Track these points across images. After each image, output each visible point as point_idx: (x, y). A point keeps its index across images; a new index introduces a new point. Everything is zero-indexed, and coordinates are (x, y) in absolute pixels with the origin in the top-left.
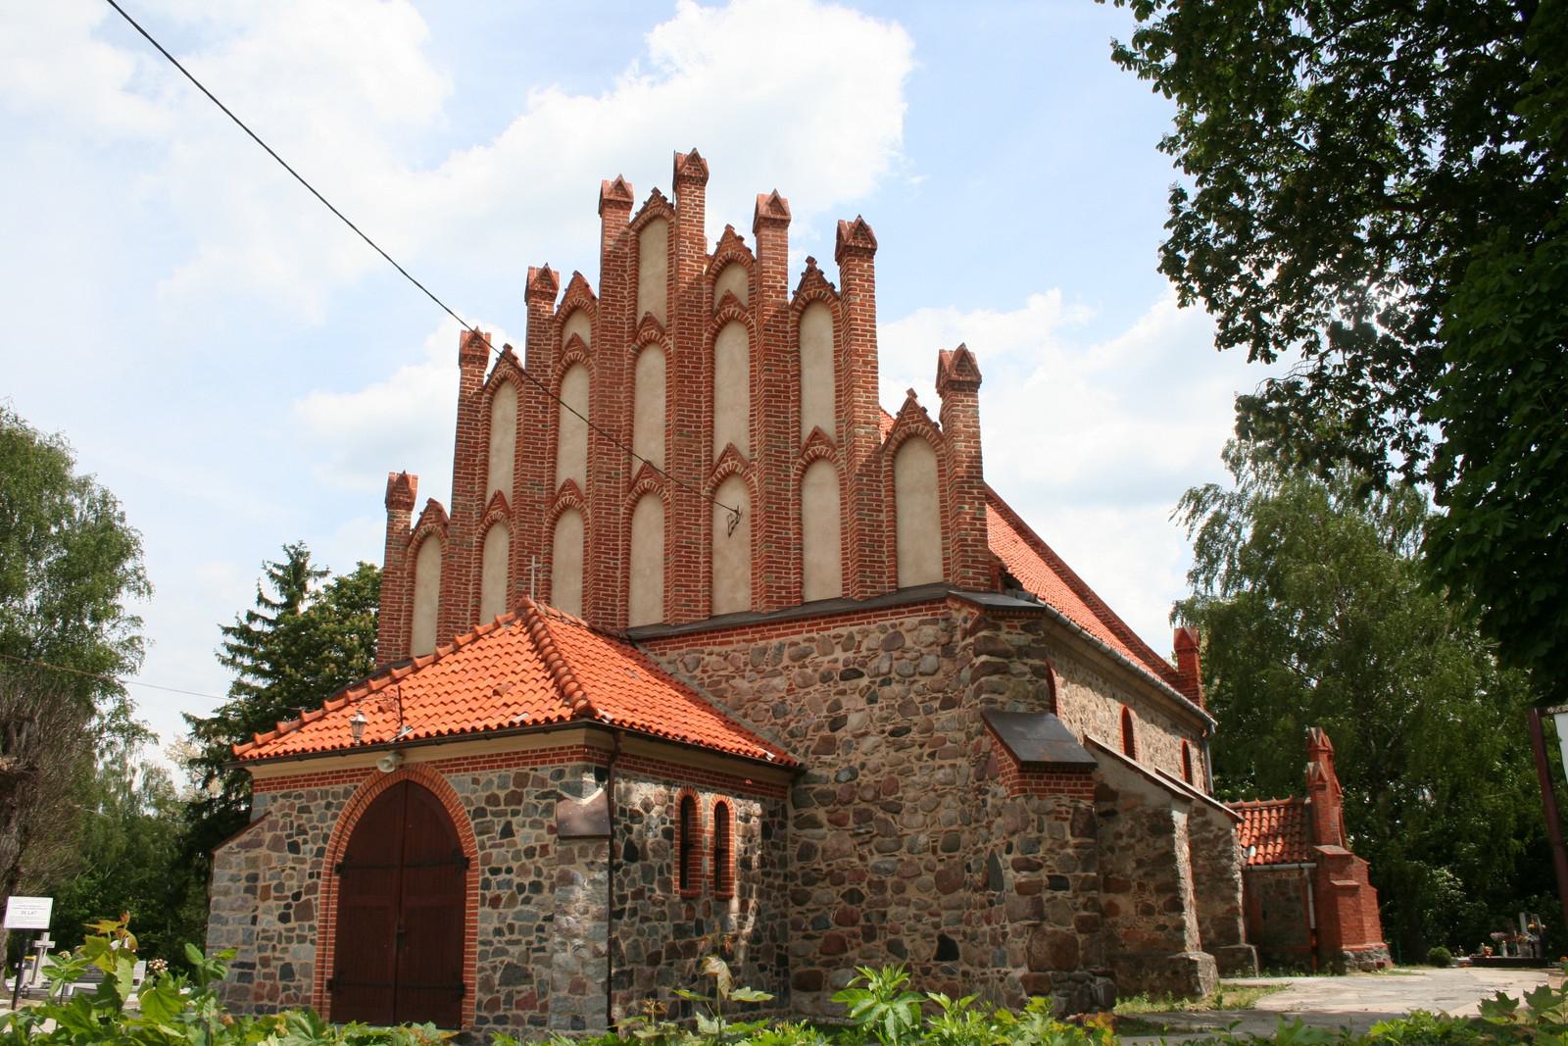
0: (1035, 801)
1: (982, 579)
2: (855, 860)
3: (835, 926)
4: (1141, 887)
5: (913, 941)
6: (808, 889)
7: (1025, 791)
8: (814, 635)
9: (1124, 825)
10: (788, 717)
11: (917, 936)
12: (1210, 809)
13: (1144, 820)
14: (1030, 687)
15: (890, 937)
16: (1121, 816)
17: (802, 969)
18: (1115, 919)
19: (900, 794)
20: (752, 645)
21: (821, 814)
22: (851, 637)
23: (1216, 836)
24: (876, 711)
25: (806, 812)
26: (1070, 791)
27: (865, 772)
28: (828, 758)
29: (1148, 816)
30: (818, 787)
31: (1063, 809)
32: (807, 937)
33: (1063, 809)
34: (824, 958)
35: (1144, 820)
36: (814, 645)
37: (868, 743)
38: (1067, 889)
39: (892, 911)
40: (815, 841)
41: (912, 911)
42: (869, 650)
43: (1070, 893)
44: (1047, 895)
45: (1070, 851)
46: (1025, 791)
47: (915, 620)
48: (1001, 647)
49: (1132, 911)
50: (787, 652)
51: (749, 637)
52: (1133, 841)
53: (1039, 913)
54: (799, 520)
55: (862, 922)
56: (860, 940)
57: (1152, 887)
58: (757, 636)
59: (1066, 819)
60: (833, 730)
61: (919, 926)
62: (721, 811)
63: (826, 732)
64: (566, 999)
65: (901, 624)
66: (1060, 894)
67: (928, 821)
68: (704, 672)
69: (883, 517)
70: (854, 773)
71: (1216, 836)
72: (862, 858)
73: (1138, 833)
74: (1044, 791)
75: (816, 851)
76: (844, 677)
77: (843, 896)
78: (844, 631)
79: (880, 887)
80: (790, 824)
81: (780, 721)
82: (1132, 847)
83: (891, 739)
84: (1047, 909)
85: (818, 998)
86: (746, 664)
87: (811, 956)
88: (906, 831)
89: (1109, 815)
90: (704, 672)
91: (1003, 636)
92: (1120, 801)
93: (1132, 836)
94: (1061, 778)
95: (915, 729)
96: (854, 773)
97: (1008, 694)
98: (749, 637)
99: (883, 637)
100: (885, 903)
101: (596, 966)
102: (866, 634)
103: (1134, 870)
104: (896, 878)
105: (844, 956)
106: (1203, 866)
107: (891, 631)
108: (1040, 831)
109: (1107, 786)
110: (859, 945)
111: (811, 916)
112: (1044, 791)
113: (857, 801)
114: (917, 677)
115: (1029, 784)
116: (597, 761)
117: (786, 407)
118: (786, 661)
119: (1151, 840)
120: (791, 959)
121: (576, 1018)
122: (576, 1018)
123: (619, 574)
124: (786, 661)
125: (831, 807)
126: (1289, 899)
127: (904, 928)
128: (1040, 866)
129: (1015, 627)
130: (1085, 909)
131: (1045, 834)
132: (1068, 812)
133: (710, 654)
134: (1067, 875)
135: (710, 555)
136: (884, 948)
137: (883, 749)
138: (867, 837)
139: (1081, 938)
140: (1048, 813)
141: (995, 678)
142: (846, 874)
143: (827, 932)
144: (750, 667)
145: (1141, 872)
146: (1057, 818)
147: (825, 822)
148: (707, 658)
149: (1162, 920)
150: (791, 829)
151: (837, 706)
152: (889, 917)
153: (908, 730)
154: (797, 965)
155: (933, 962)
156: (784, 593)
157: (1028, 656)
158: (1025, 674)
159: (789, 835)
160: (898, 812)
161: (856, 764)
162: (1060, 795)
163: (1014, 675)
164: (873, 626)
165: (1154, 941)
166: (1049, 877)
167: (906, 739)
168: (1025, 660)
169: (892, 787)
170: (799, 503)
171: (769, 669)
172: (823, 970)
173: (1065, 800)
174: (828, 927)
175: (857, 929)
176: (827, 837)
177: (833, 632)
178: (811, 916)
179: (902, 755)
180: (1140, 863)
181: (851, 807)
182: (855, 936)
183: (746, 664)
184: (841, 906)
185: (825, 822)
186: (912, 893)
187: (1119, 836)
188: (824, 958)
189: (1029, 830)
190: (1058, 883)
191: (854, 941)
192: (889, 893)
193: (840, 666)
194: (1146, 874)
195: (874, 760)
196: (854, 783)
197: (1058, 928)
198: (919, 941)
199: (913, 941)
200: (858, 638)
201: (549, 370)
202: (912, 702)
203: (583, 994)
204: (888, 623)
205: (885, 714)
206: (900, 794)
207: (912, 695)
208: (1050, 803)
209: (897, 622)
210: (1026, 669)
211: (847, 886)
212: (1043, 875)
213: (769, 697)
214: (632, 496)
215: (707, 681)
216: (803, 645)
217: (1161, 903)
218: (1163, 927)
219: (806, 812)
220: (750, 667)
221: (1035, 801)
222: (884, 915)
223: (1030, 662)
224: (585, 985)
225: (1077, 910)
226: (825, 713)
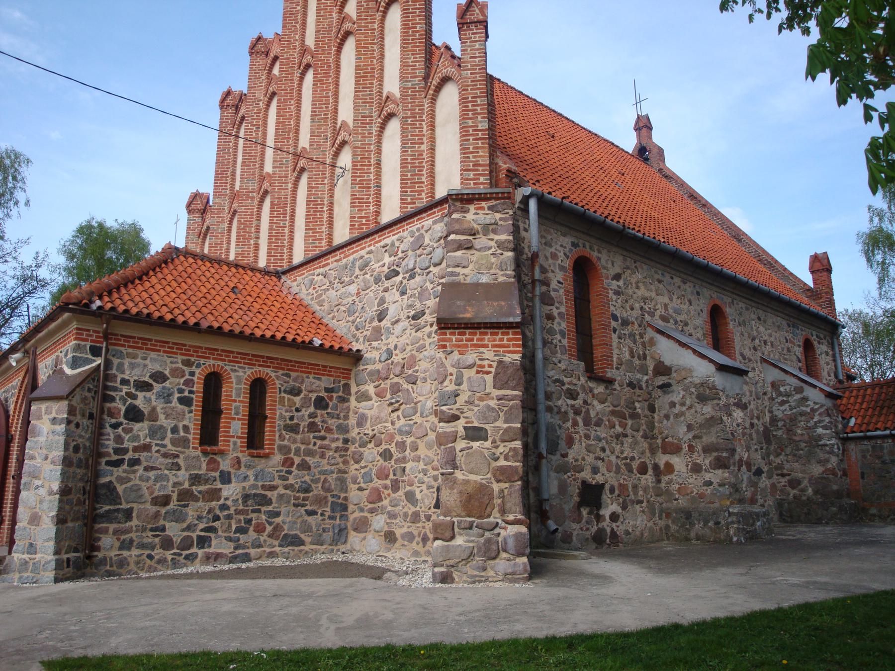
0: (456, 356)
1: (482, 179)
2: (389, 424)
3: (376, 480)
4: (691, 448)
5: (421, 491)
6: (362, 450)
7: (444, 347)
8: (372, 248)
9: (676, 396)
10: (356, 315)
11: (424, 487)
12: (805, 386)
13: (693, 390)
14: (493, 260)
15: (408, 488)
16: (674, 388)
17: (357, 514)
18: (670, 477)
19: (417, 368)
20: (340, 263)
21: (370, 389)
22: (393, 244)
23: (812, 410)
24: (405, 301)
25: (363, 388)
26: (493, 346)
27: (397, 352)
28: (375, 344)
29: (695, 386)
30: (370, 367)
31: (486, 363)
32: (361, 489)
33: (486, 363)
34: (370, 506)
35: (693, 390)
36: (371, 256)
37: (398, 328)
38: (486, 439)
39: (409, 466)
40: (366, 412)
41: (422, 466)
42: (403, 252)
43: (488, 444)
44: (461, 444)
45: (493, 403)
46: (444, 347)
47: (430, 222)
48: (466, 226)
49: (684, 469)
50: (358, 264)
51: (337, 258)
52: (684, 409)
53: (452, 462)
54: (378, 164)
55: (391, 476)
56: (390, 491)
57: (699, 448)
58: (342, 256)
59: (488, 373)
60: (380, 321)
61: (426, 479)
62: (258, 388)
63: (376, 323)
64: (25, 528)
65: (423, 227)
66: (476, 445)
67: (433, 389)
68: (314, 289)
69: (424, 147)
70: (390, 354)
71: (812, 410)
72: (393, 423)
73: (688, 403)
74: (466, 346)
75: (367, 419)
76: (388, 278)
77: (381, 455)
78: (388, 241)
79: (402, 446)
80: (353, 399)
81: (351, 319)
82: (682, 414)
83: (413, 322)
84: (460, 459)
85: (364, 538)
86: (335, 278)
87: (362, 505)
88: (419, 398)
89: (665, 387)
90: (314, 289)
91: (470, 216)
92: (674, 375)
93: (683, 404)
94: (486, 334)
95: (427, 311)
96: (390, 354)
97: (471, 266)
98: (337, 258)
99: (412, 239)
100: (404, 460)
101: (50, 501)
102: (401, 240)
103: (685, 434)
104: (412, 439)
105: (380, 504)
106: (802, 435)
107: (417, 234)
108: (459, 384)
109: (663, 363)
110: (389, 495)
111: (363, 471)
112: (466, 346)
113: (392, 376)
114: (432, 268)
115: (450, 340)
116: (92, 341)
117: (372, 84)
118: (357, 272)
119: (698, 407)
120: (351, 507)
121: (31, 545)
122: (31, 545)
123: (286, 230)
124: (357, 272)
125: (377, 383)
126: (884, 462)
127: (416, 480)
128: (455, 418)
129: (482, 208)
130: (506, 459)
131: (464, 387)
132: (490, 366)
133: (318, 275)
134: (486, 426)
135: (331, 204)
136: (404, 497)
137: (408, 331)
138: (397, 405)
139: (496, 487)
140: (470, 367)
141: (459, 253)
142: (383, 436)
143: (371, 485)
144: (337, 280)
145: (690, 435)
146: (478, 372)
147: (373, 395)
148: (316, 278)
149: (708, 476)
150: (353, 402)
151: (382, 301)
152: (407, 471)
153: (423, 313)
154: (354, 512)
155: (433, 510)
156: (364, 221)
157: (495, 232)
158: (490, 248)
159: (352, 407)
160: (414, 383)
161: (391, 346)
162: (482, 350)
163: (479, 250)
164: (406, 233)
165: (701, 496)
166: (465, 428)
167: (421, 321)
168: (492, 236)
169: (412, 362)
170: (379, 152)
171: (349, 279)
172: (368, 515)
173: (489, 354)
174: (371, 481)
175: (388, 482)
176: (373, 408)
177: (382, 244)
178: (363, 471)
179: (419, 334)
180: (690, 427)
181: (388, 382)
182: (386, 487)
183: (335, 278)
184: (379, 464)
185: (373, 395)
186: (422, 451)
187: (673, 405)
188: (370, 506)
189: (446, 383)
190: (475, 434)
191: (386, 492)
192: (408, 451)
193: (386, 269)
194: (695, 437)
195: (403, 340)
196: (390, 361)
197: (473, 477)
198: (425, 491)
199: (421, 491)
200: (397, 244)
201: (261, 103)
202: (427, 289)
203: (37, 525)
204: (414, 228)
205: (410, 302)
206: (417, 368)
207: (428, 284)
208: (471, 357)
209: (420, 226)
210: (493, 244)
211: (384, 447)
212: (459, 426)
213: (345, 302)
214: (295, 174)
215: (315, 295)
216: (366, 256)
217: (707, 462)
218: (709, 483)
219: (363, 388)
220: (337, 280)
221: (456, 356)
222: (404, 470)
223: (496, 237)
224: (40, 517)
225: (496, 459)
226: (376, 308)
